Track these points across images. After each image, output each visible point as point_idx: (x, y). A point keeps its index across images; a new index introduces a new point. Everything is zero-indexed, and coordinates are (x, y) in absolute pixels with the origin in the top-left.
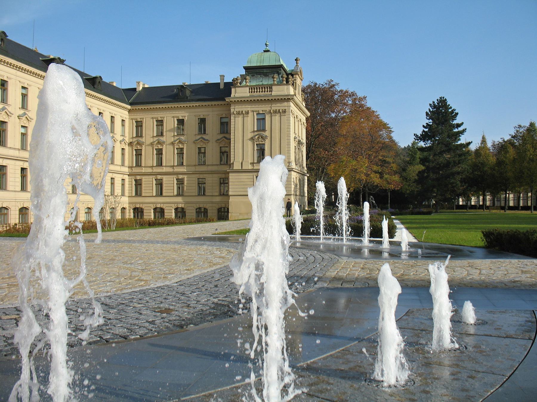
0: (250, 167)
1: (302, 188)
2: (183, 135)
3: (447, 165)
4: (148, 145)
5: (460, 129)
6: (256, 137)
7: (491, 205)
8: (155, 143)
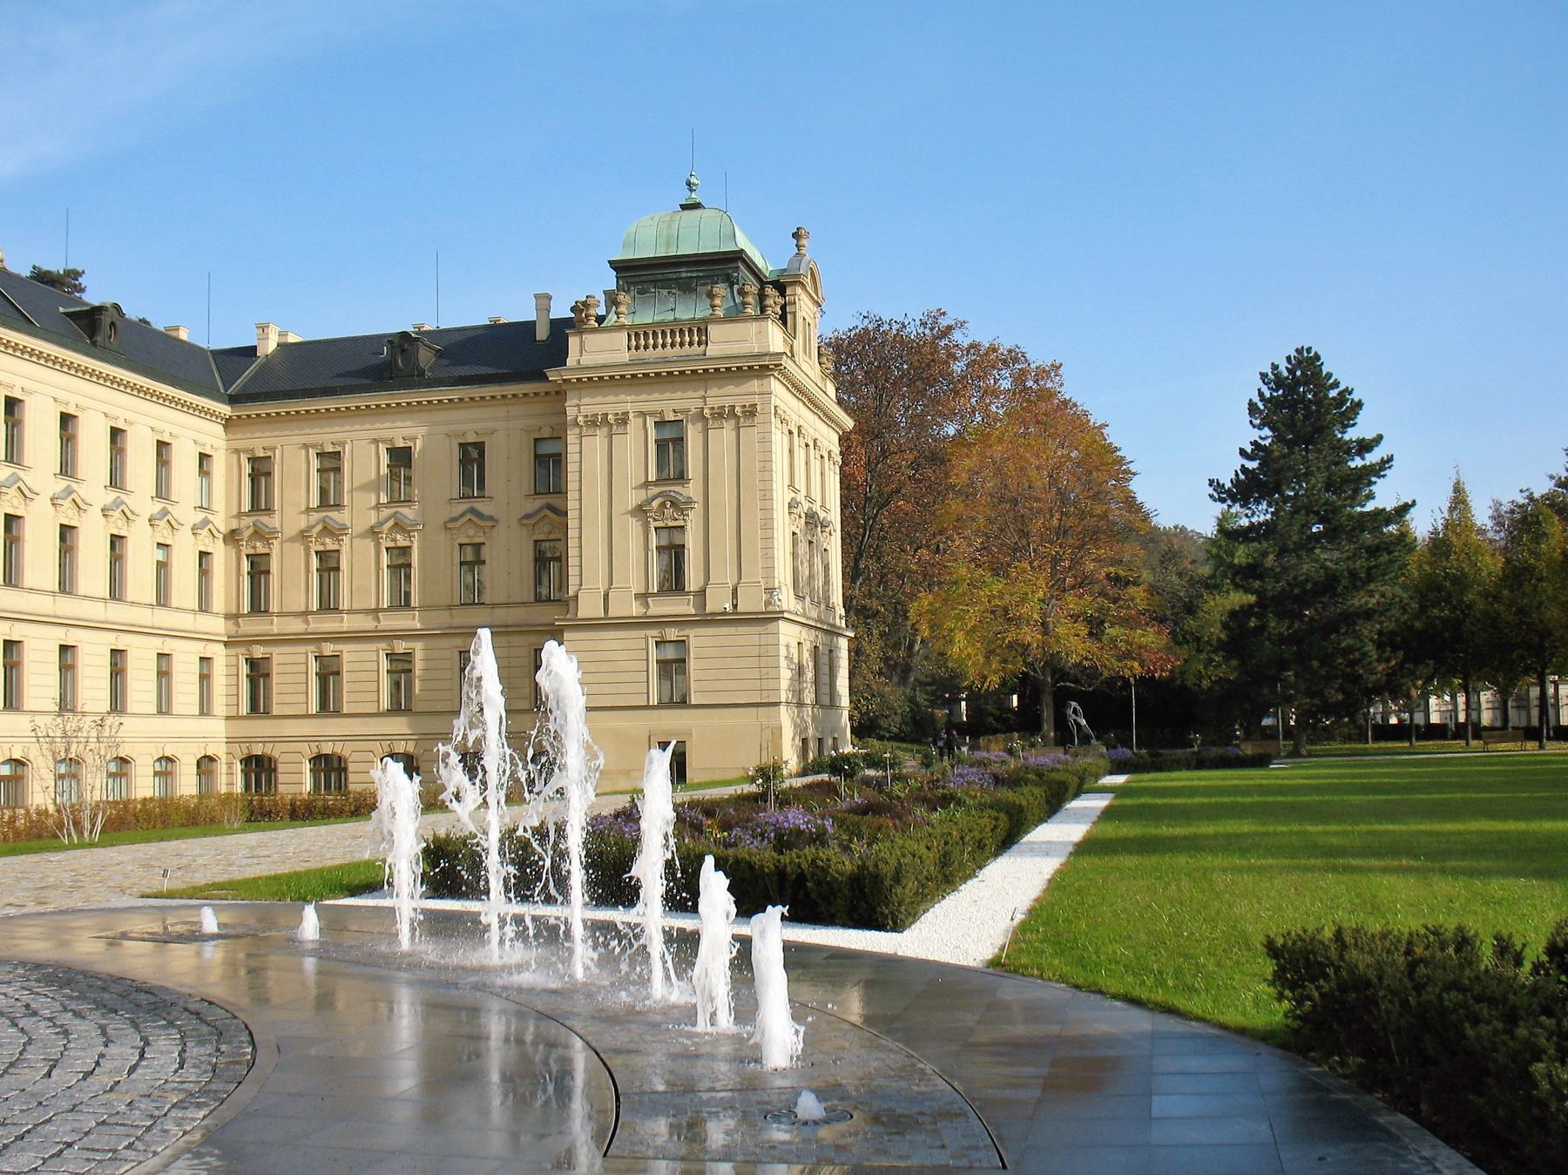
0: (636, 609)
1: (825, 679)
2: (409, 501)
3: (1328, 585)
4: (292, 540)
5: (1372, 458)
6: (655, 504)
7: (1498, 724)
8: (315, 532)
